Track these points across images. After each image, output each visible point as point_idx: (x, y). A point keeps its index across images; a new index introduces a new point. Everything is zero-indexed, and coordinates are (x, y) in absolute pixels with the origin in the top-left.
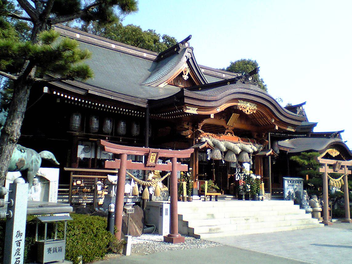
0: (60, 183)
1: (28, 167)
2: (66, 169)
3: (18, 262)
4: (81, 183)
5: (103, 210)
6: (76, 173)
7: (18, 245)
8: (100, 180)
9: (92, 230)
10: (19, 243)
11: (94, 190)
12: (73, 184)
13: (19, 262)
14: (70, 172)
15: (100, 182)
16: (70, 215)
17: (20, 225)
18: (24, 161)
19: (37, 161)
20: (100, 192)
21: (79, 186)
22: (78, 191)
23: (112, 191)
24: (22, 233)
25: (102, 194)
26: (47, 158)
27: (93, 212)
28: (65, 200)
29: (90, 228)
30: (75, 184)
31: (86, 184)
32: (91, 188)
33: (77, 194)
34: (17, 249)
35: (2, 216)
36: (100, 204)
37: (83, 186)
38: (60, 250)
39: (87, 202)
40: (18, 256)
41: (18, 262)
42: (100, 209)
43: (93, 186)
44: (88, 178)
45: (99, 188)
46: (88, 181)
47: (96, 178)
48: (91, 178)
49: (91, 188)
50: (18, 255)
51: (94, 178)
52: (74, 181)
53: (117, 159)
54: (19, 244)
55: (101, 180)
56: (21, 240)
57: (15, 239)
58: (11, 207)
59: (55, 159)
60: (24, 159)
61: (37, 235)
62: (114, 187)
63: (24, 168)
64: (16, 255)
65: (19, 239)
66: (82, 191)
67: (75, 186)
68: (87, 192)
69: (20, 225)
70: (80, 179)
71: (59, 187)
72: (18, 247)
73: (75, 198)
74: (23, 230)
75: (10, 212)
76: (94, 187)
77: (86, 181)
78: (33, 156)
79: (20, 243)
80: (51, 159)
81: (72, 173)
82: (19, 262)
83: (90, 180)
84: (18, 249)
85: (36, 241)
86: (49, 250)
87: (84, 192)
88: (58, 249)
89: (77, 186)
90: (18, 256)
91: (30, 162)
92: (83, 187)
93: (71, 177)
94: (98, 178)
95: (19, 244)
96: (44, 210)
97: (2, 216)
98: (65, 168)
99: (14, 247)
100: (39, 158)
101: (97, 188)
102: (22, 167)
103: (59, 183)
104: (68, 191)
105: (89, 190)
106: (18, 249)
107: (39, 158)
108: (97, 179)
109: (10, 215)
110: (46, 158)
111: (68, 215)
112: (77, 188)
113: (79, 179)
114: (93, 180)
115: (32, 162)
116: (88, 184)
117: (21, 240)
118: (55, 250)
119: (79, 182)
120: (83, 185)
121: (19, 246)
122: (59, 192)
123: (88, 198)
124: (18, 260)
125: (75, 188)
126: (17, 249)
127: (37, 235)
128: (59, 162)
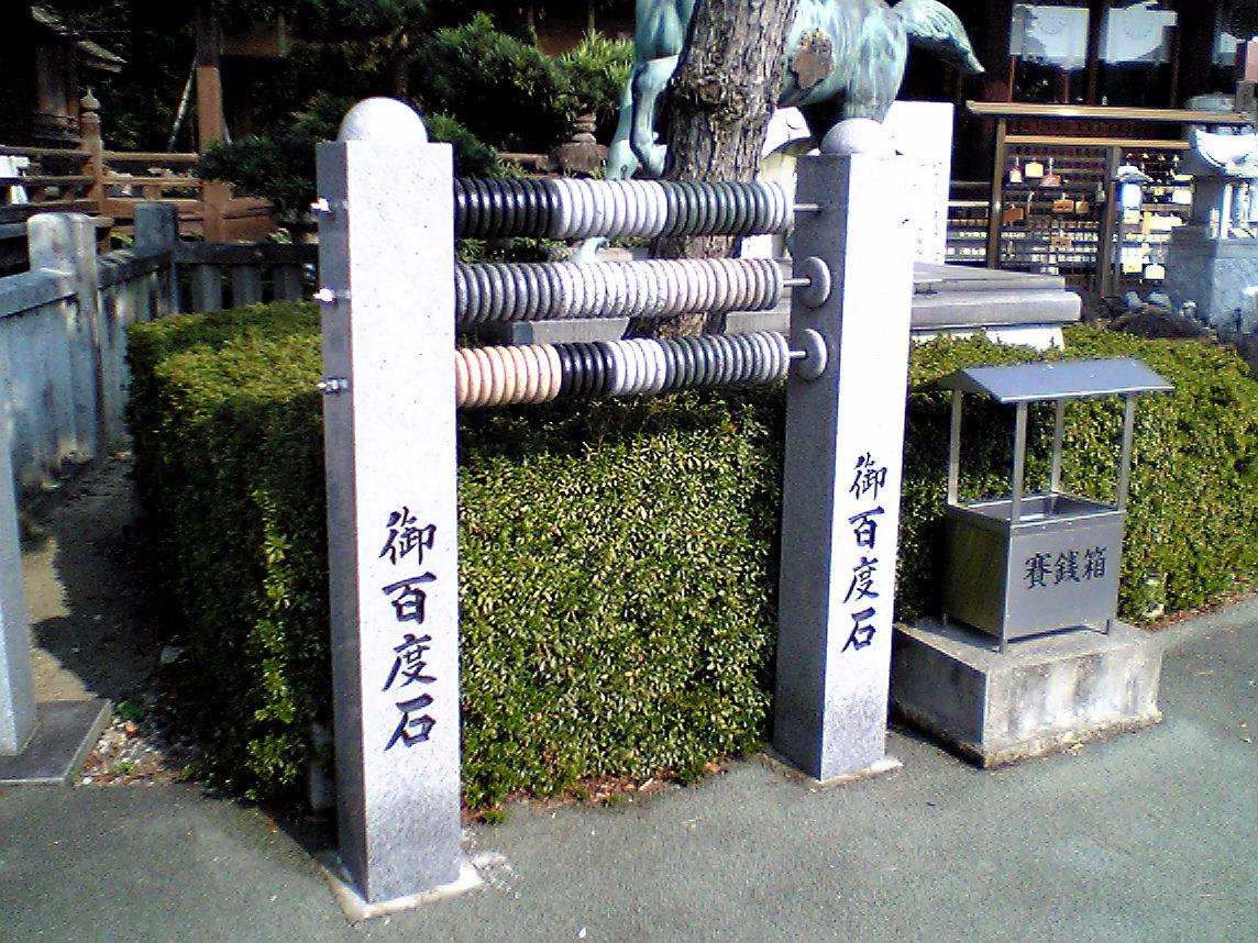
0: (956, 174)
1: (845, 80)
2: (975, 107)
3: (865, 634)
4: (1045, 173)
5: (1168, 304)
6: (1018, 124)
7: (865, 537)
8: (1133, 157)
9: (1229, 436)
10: (867, 527)
11: (1104, 206)
12: (1006, 179)
13: (870, 637)
14: (996, 117)
15: (1130, 169)
16: (1069, 340)
17: (870, 422)
18: (826, 47)
19: (888, 46)
20: (1131, 217)
21: (1033, 189)
22: (1032, 210)
23: (1214, 214)
24: (885, 470)
25: (1138, 228)
26: (929, 34)
27: (1121, 313)
28: (966, 251)
29: (1218, 426)
30: (1016, 177)
31: (1067, 176)
32: (1091, 198)
33: (1020, 225)
34: (859, 564)
35: (766, 374)
36: (1130, 271)
37: (1050, 189)
38: (1095, 568)
39: (1062, 258)
40: (867, 602)
41: (865, 634)
42: (1155, 297)
43: (1100, 188)
44: (1078, 150)
45: (1131, 196)
46: (1078, 165)
47: (1111, 147)
48: (1088, 151)
49: (1091, 198)
50: (865, 592)
51: (1104, 152)
52: (1011, 164)
53: (976, 100)
54: (867, 532)
55: (1136, 162)
56: (880, 510)
57: (845, 505)
58: (815, 309)
59: (964, 43)
60: (825, 34)
61: (954, 468)
62: (1228, 190)
63: (829, 86)
64: (856, 593)
65: (867, 502)
66: (1049, 211)
67: (1017, 187)
68: (1073, 216)
69: (870, 422)
70: (1040, 153)
71: (955, 194)
72: (865, 551)
73: (1016, 242)
74: (890, 452)
75: (812, 343)
76: (1103, 194)
77: (1069, 165)
78: (867, 20)
79: (873, 525)
80: (949, 42)
81: (1002, 127)
82: (870, 637)
83: (1083, 159)
84: (864, 560)
85: (952, 501)
86: (1037, 565)
87: (1055, 216)
88: (1081, 562)
89: (1025, 189)
90: (867, 602)
91: (854, 53)
92: (1053, 193)
93: (999, 146)
94: (1125, 150)
95: (867, 532)
96: (958, 309)
97: (766, 374)
98: (969, 102)
99: (844, 554)
100: (896, 33)
101: (1118, 198)
102: (820, 81)
103: (953, 177)
104: (979, 212)
105: (1078, 204)
106: (864, 560)
107: (896, 33)
108: (1117, 154)
109: (812, 356)
110: (925, 33)
111: (1057, 335)
112: (1025, 199)
113: (1036, 152)
114: (1101, 160)
115: (865, 50)
116: (1077, 177)
117: (880, 510)
118: (1067, 568)
119: (1034, 170)
120: (1051, 181)
121: (871, 542)
122: (953, 213)
123: (1074, 244)
124: (862, 624)
125: (1016, 199)
126: (859, 564)
127: (954, 468)
128: (982, 63)
